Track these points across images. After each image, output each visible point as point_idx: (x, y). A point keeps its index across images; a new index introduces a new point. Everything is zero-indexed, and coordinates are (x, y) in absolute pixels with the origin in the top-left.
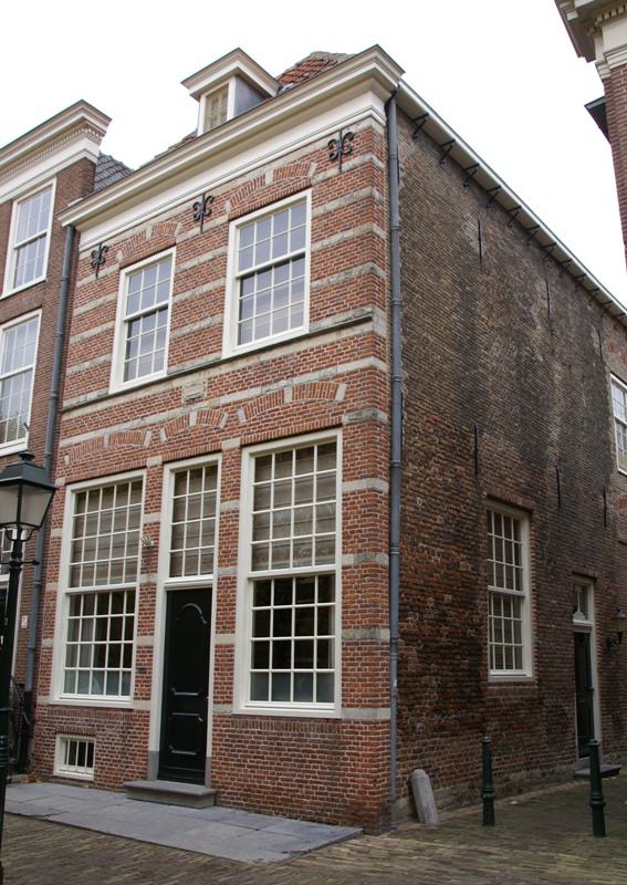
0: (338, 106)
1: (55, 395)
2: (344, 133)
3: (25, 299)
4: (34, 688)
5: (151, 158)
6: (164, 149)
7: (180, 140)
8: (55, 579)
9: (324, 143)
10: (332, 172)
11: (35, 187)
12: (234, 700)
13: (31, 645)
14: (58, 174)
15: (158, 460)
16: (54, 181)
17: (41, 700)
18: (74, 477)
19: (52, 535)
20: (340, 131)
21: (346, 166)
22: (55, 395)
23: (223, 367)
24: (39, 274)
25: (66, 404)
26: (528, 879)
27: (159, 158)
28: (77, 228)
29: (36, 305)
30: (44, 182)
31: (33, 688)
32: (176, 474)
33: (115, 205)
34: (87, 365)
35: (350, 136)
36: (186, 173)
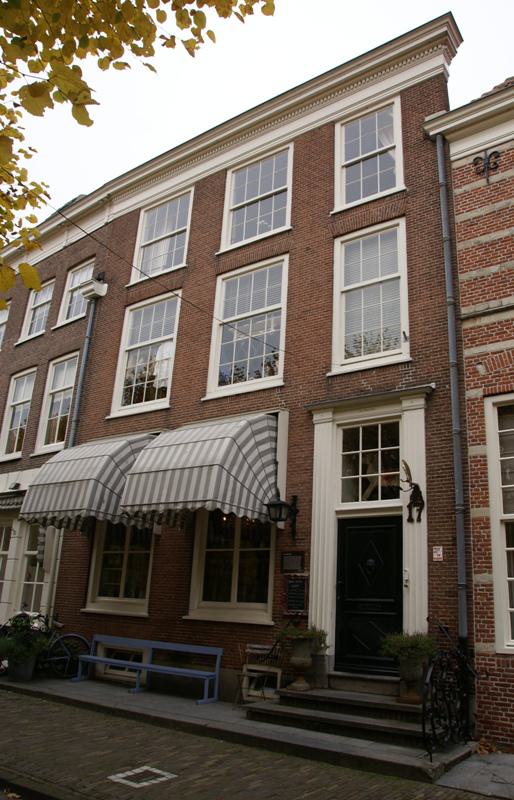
0: (476, 133)
1: (452, 300)
2: (489, 152)
3: (143, 288)
4: (470, 633)
5: (479, 96)
6: (489, 89)
7: (502, 81)
8: (486, 504)
9: (471, 159)
10: (482, 182)
11: (367, 108)
12: (497, 638)
13: (462, 581)
14: (401, 93)
15: (479, 393)
16: (193, 189)
17: (480, 647)
18: (498, 388)
19: (470, 454)
20: (485, 150)
21: (494, 178)
22: (452, 300)
23: (483, 319)
24: (181, 262)
25: (464, 311)
26: (499, 767)
27: (474, 103)
28: (447, 137)
29: (284, 250)
30: (281, 145)
31: (469, 634)
32: (345, 431)
33: (509, 110)
34: (495, 269)
35: (496, 154)
36: (496, 118)
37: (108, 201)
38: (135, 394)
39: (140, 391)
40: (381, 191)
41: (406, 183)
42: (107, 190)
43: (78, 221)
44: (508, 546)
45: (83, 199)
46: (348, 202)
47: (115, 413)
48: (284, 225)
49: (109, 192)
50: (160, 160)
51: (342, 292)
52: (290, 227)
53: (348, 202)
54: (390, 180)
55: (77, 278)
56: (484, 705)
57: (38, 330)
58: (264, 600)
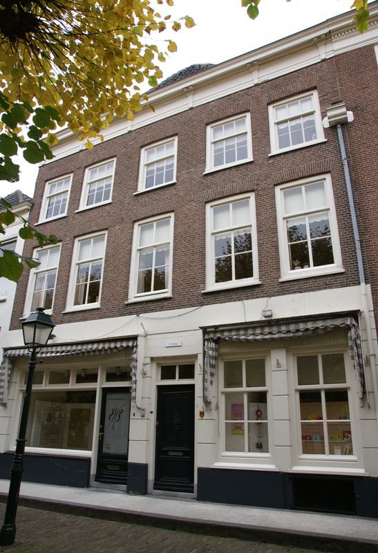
28: (29, 208)
37: (327, 38)
38: (299, 257)
39: (152, 280)
40: (96, 202)
41: (177, 180)
42: (328, 26)
43: (156, 105)
44: (226, 420)
45: (208, 67)
46: (215, 165)
47: (131, 299)
48: (172, 180)
49: (331, 28)
50: (236, 60)
51: (212, 234)
52: (252, 160)
53: (215, 165)
54: (243, 154)
55: (52, 187)
56: (99, 525)
57: (62, 212)
58: (200, 469)
